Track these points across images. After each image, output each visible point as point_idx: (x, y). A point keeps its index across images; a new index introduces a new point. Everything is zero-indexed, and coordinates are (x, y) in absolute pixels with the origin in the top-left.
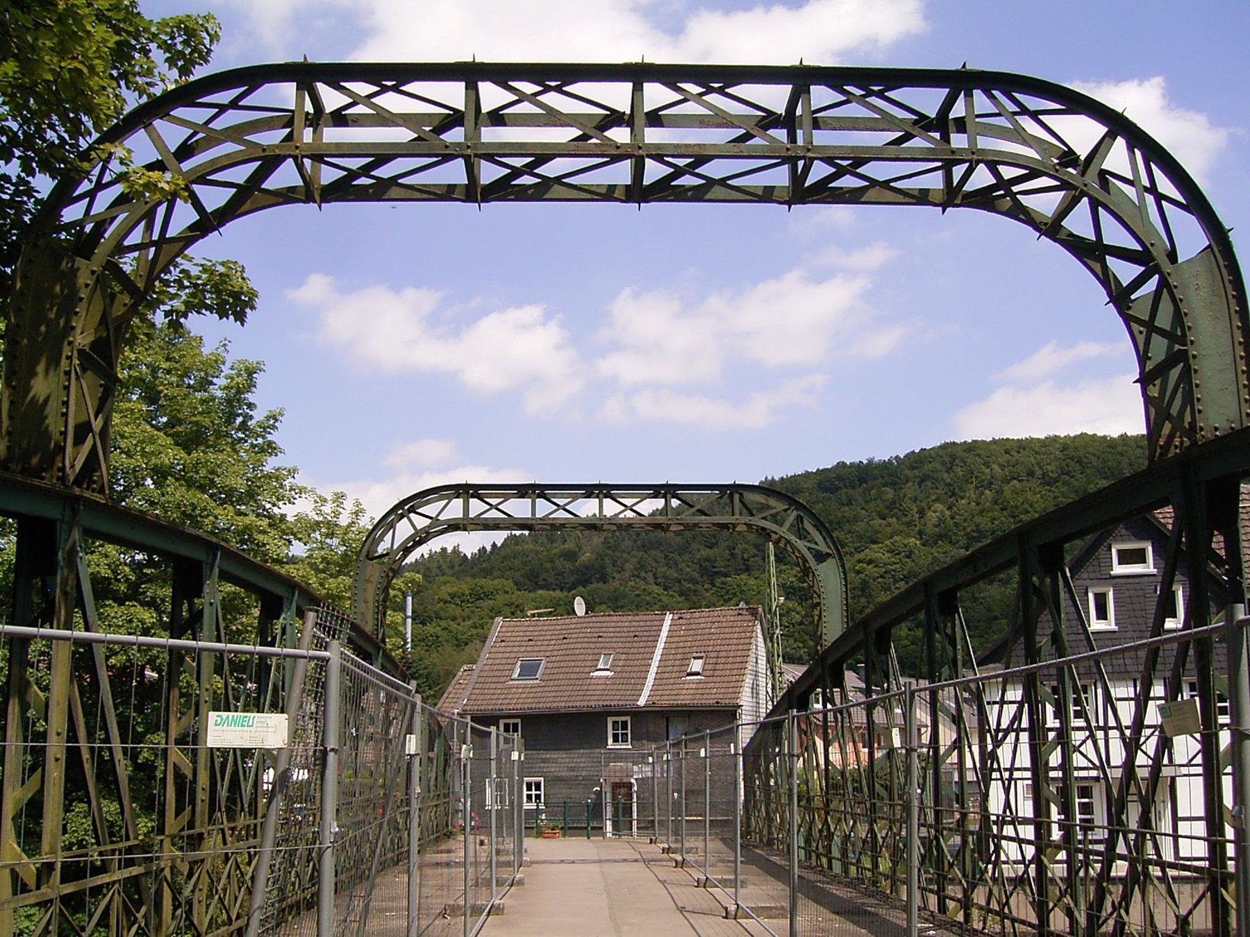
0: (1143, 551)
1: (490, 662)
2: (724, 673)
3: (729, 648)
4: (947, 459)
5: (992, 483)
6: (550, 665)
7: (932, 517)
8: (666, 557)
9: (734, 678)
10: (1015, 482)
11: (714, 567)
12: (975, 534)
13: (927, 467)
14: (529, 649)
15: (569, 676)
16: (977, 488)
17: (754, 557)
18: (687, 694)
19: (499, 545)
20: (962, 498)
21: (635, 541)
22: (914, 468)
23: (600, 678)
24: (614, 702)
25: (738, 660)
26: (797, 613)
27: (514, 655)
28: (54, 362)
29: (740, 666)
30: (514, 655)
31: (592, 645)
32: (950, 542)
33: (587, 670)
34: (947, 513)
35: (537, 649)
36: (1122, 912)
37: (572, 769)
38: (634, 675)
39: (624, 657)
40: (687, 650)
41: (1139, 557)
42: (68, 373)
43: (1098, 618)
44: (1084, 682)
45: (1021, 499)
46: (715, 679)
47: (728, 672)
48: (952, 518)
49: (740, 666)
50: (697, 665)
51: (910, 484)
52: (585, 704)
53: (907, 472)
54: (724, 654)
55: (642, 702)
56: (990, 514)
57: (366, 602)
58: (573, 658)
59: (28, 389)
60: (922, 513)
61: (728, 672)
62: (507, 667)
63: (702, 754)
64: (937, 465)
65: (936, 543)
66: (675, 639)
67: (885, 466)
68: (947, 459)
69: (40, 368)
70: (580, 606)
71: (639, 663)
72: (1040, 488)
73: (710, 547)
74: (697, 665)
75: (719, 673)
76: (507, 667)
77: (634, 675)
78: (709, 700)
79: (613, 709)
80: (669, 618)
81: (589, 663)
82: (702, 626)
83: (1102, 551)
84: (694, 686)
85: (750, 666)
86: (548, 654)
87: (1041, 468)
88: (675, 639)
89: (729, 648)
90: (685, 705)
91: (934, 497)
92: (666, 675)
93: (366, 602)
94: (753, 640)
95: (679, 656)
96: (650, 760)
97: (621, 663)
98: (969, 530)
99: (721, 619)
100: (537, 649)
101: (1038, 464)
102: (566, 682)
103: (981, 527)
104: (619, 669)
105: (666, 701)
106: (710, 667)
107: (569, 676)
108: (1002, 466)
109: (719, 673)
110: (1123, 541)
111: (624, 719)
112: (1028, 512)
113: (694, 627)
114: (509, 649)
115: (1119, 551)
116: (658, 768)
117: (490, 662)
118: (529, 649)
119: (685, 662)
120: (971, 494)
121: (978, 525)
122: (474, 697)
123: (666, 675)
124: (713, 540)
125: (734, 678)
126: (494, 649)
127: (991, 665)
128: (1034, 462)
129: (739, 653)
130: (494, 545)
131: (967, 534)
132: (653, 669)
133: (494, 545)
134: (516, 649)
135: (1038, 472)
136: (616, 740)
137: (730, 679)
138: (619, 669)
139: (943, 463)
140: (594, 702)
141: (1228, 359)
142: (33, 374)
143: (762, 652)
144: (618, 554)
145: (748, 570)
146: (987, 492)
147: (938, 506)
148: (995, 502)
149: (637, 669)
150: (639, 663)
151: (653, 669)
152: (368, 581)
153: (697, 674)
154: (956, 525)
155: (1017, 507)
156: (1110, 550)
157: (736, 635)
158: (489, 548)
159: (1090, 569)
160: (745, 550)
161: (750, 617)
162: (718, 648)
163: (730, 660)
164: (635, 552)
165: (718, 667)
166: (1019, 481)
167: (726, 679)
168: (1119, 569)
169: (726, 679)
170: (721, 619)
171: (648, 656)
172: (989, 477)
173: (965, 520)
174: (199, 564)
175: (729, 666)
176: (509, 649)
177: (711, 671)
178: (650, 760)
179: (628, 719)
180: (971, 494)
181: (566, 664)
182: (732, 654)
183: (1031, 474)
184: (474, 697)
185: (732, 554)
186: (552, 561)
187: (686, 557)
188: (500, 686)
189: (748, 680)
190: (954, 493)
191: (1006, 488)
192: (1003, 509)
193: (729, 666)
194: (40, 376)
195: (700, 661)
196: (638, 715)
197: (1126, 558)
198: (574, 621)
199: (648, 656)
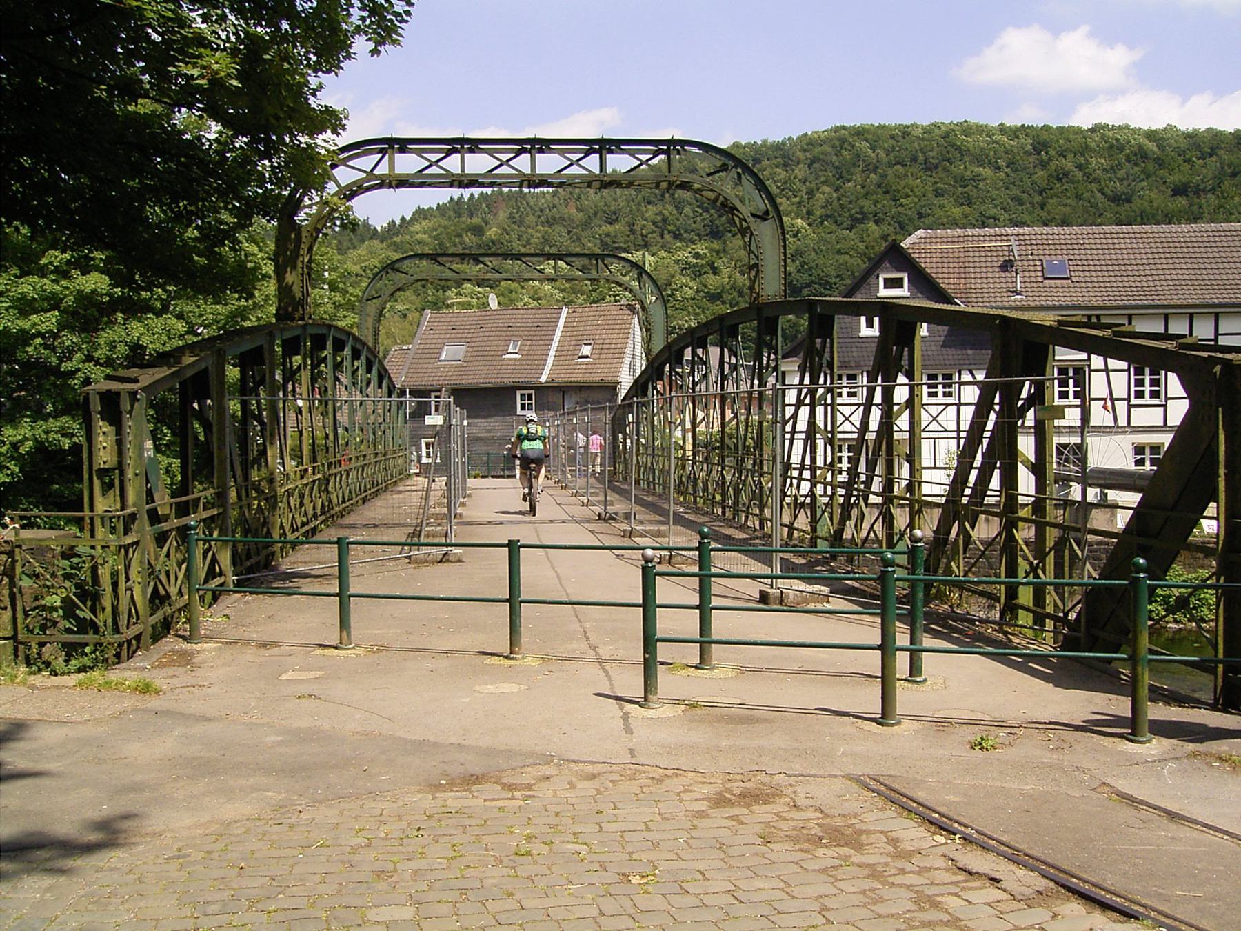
0: (901, 279)
1: (422, 346)
2: (608, 356)
3: (612, 336)
4: (837, 144)
5: (877, 167)
6: (471, 350)
7: (820, 198)
8: (569, 232)
9: (615, 361)
10: (899, 166)
11: (614, 242)
12: (859, 216)
13: (816, 151)
14: (453, 336)
15: (485, 358)
16: (863, 171)
17: (652, 233)
18: (578, 373)
19: (408, 218)
20: (849, 181)
21: (539, 217)
22: (805, 151)
23: (510, 360)
24: (522, 379)
25: (619, 346)
26: (691, 288)
27: (440, 341)
28: (294, 267)
29: (620, 351)
30: (440, 341)
31: (503, 333)
32: (836, 222)
33: (499, 353)
34: (835, 195)
35: (459, 336)
36: (1040, 572)
37: (489, 431)
38: (538, 357)
39: (529, 343)
40: (579, 338)
41: (897, 283)
42: (302, 275)
43: (867, 327)
44: (840, 372)
45: (903, 183)
46: (600, 361)
47: (611, 356)
48: (839, 199)
49: (620, 351)
50: (586, 350)
51: (801, 166)
52: (499, 380)
53: (798, 153)
54: (608, 341)
55: (543, 379)
56: (874, 197)
57: (367, 328)
58: (489, 343)
59: (284, 279)
60: (811, 193)
61: (611, 356)
62: (435, 351)
63: (575, 421)
64: (829, 150)
65: (822, 223)
66: (570, 329)
67: (778, 147)
68: (837, 144)
69: (289, 269)
70: (493, 302)
71: (541, 348)
72: (921, 173)
73: (610, 223)
74: (586, 350)
75: (604, 356)
76: (435, 351)
77: (538, 357)
78: (595, 378)
79: (520, 385)
80: (565, 311)
81: (501, 348)
82: (591, 318)
83: (872, 280)
84: (584, 367)
85: (629, 351)
86: (468, 340)
87: (924, 154)
88: (570, 329)
89: (612, 336)
90: (577, 382)
91: (823, 179)
92: (562, 358)
93: (367, 328)
94: (631, 331)
95: (572, 343)
96: (547, 424)
97: (527, 348)
98: (853, 211)
99: (606, 313)
100: (459, 336)
101: (921, 150)
102: (484, 363)
103: (865, 210)
104: (525, 353)
105: (562, 378)
106: (597, 351)
107: (485, 358)
108: (888, 153)
109: (604, 356)
110: (888, 272)
111: (530, 392)
112: (909, 196)
113: (585, 319)
114: (437, 336)
115: (885, 279)
116: (552, 429)
117: (422, 346)
118: (453, 336)
119: (578, 347)
120: (858, 177)
121: (862, 208)
122: (410, 375)
123: (562, 358)
124: (614, 217)
125: (615, 361)
126: (424, 337)
127: (790, 359)
128: (918, 148)
129: (620, 341)
130: (403, 219)
131: (851, 216)
132: (552, 353)
133: (403, 219)
134: (442, 336)
135: (921, 157)
136: (523, 408)
137: (612, 361)
138: (525, 353)
139: (834, 147)
140: (507, 379)
141: (777, 266)
142: (286, 272)
143: (638, 339)
144: (523, 229)
145: (646, 246)
146: (872, 176)
147: (826, 189)
148: (879, 186)
149: (539, 352)
150: (541, 348)
151: (552, 353)
152: (368, 315)
153: (587, 357)
154: (842, 206)
155: (898, 191)
156: (878, 278)
157: (618, 326)
158: (398, 222)
159: (863, 291)
160: (644, 226)
161: (629, 312)
162: (603, 336)
163: (613, 346)
164: (540, 227)
165: (604, 346)
166: (903, 166)
167: (609, 361)
168: (883, 292)
169: (609, 361)
170: (606, 313)
171: (548, 342)
172: (874, 161)
173: (851, 202)
174: (325, 335)
175: (612, 351)
176: (437, 336)
177: (598, 354)
178: (547, 424)
179: (532, 392)
180: (858, 177)
181: (483, 348)
182: (614, 341)
183: (914, 159)
184: (410, 375)
185: (631, 230)
186: (460, 236)
187: (588, 232)
188: (430, 366)
189: (627, 361)
190: (841, 174)
191: (890, 171)
192: (887, 192)
193: (612, 351)
194: (288, 274)
195: (589, 347)
196: (540, 388)
197: (890, 283)
198: (488, 313)
199: (548, 342)
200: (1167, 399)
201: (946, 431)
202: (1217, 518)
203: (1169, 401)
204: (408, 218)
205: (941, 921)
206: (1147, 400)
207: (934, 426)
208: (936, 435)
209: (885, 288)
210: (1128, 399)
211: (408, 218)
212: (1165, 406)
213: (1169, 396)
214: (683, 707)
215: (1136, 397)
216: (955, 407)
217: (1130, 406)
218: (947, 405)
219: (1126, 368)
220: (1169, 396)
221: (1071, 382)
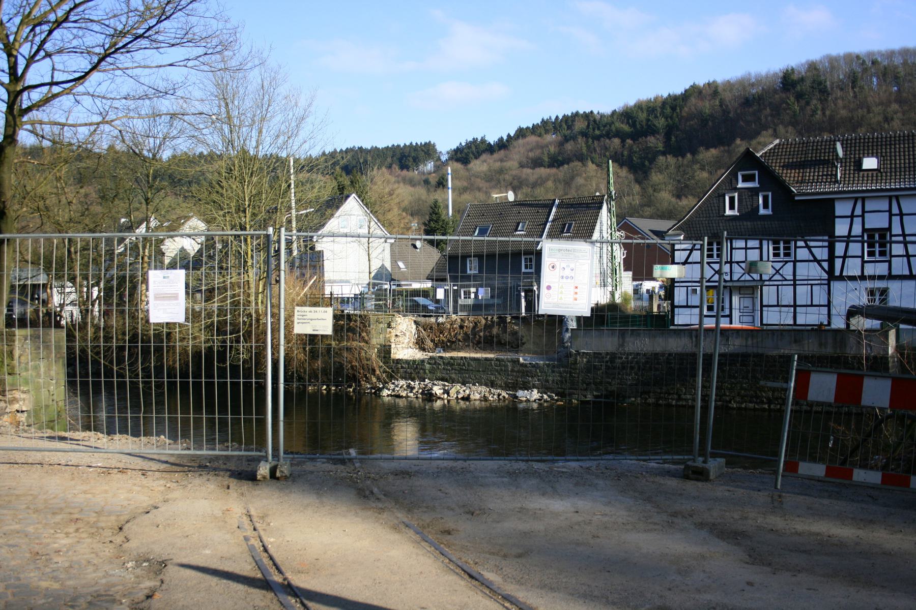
0: (754, 175)
115: (743, 176)
133: (509, 135)
136: (526, 267)
200: (891, 256)
201: (786, 280)
202: (795, 324)
203: (893, 259)
204: (512, 135)
205: (683, 517)
206: (878, 258)
207: (777, 277)
208: (780, 283)
209: (743, 181)
210: (862, 257)
211: (512, 135)
212: (890, 262)
213: (893, 254)
214: (104, 36)
215: (869, 255)
216: (792, 263)
217: (863, 262)
218: (786, 262)
219: (758, 246)
220: (893, 254)
221: (877, 245)
